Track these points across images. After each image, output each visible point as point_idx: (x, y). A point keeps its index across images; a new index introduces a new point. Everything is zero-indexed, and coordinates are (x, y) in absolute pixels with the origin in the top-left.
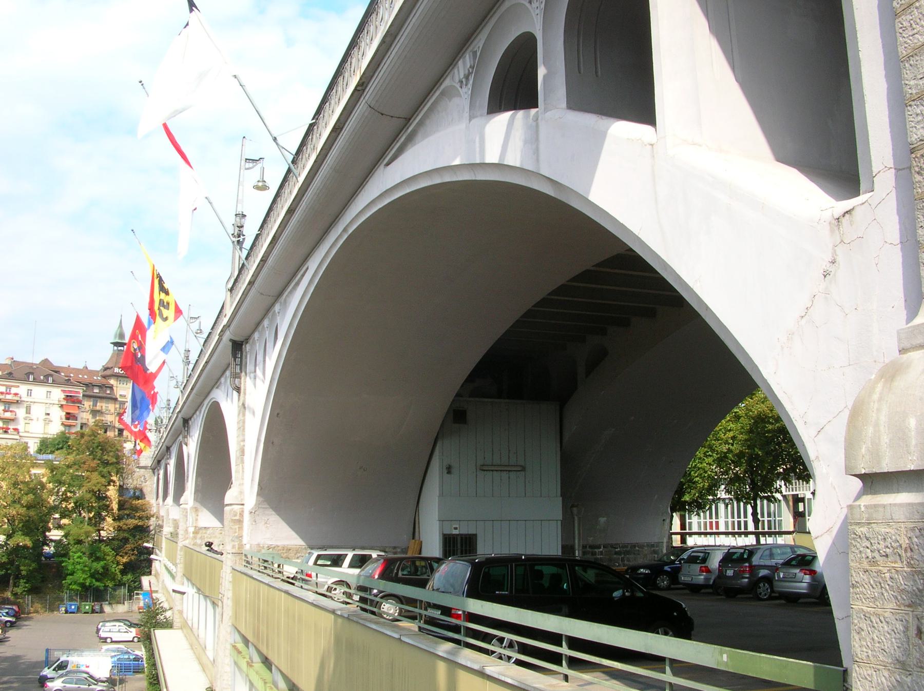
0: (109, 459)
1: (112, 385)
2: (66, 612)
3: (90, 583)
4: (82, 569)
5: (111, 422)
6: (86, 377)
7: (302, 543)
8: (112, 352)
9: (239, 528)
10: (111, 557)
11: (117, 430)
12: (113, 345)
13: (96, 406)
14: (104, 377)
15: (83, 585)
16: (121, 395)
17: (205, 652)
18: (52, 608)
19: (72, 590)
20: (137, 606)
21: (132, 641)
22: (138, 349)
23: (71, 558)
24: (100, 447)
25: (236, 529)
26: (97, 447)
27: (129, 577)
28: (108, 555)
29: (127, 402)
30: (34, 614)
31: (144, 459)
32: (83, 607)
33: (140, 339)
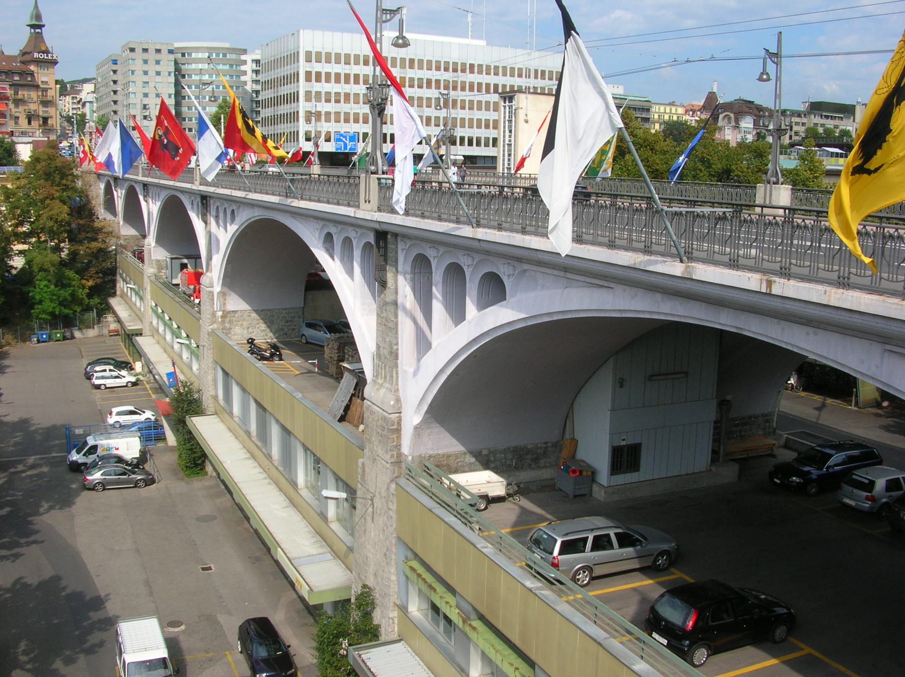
0: (68, 183)
1: (33, 71)
2: (39, 341)
3: (59, 312)
4: (49, 298)
7: (462, 448)
9: (397, 437)
10: (76, 282)
11: (41, 119)
12: (29, 28)
13: (18, 95)
14: (23, 63)
15: (52, 314)
16: (42, 82)
17: (296, 490)
18: (25, 339)
19: (41, 319)
20: (107, 329)
21: (126, 386)
22: (163, 135)
23: (37, 286)
24: (57, 172)
25: (394, 438)
26: (55, 172)
27: (96, 300)
28: (74, 280)
29: (51, 88)
30: (8, 348)
32: (54, 335)
33: (166, 124)
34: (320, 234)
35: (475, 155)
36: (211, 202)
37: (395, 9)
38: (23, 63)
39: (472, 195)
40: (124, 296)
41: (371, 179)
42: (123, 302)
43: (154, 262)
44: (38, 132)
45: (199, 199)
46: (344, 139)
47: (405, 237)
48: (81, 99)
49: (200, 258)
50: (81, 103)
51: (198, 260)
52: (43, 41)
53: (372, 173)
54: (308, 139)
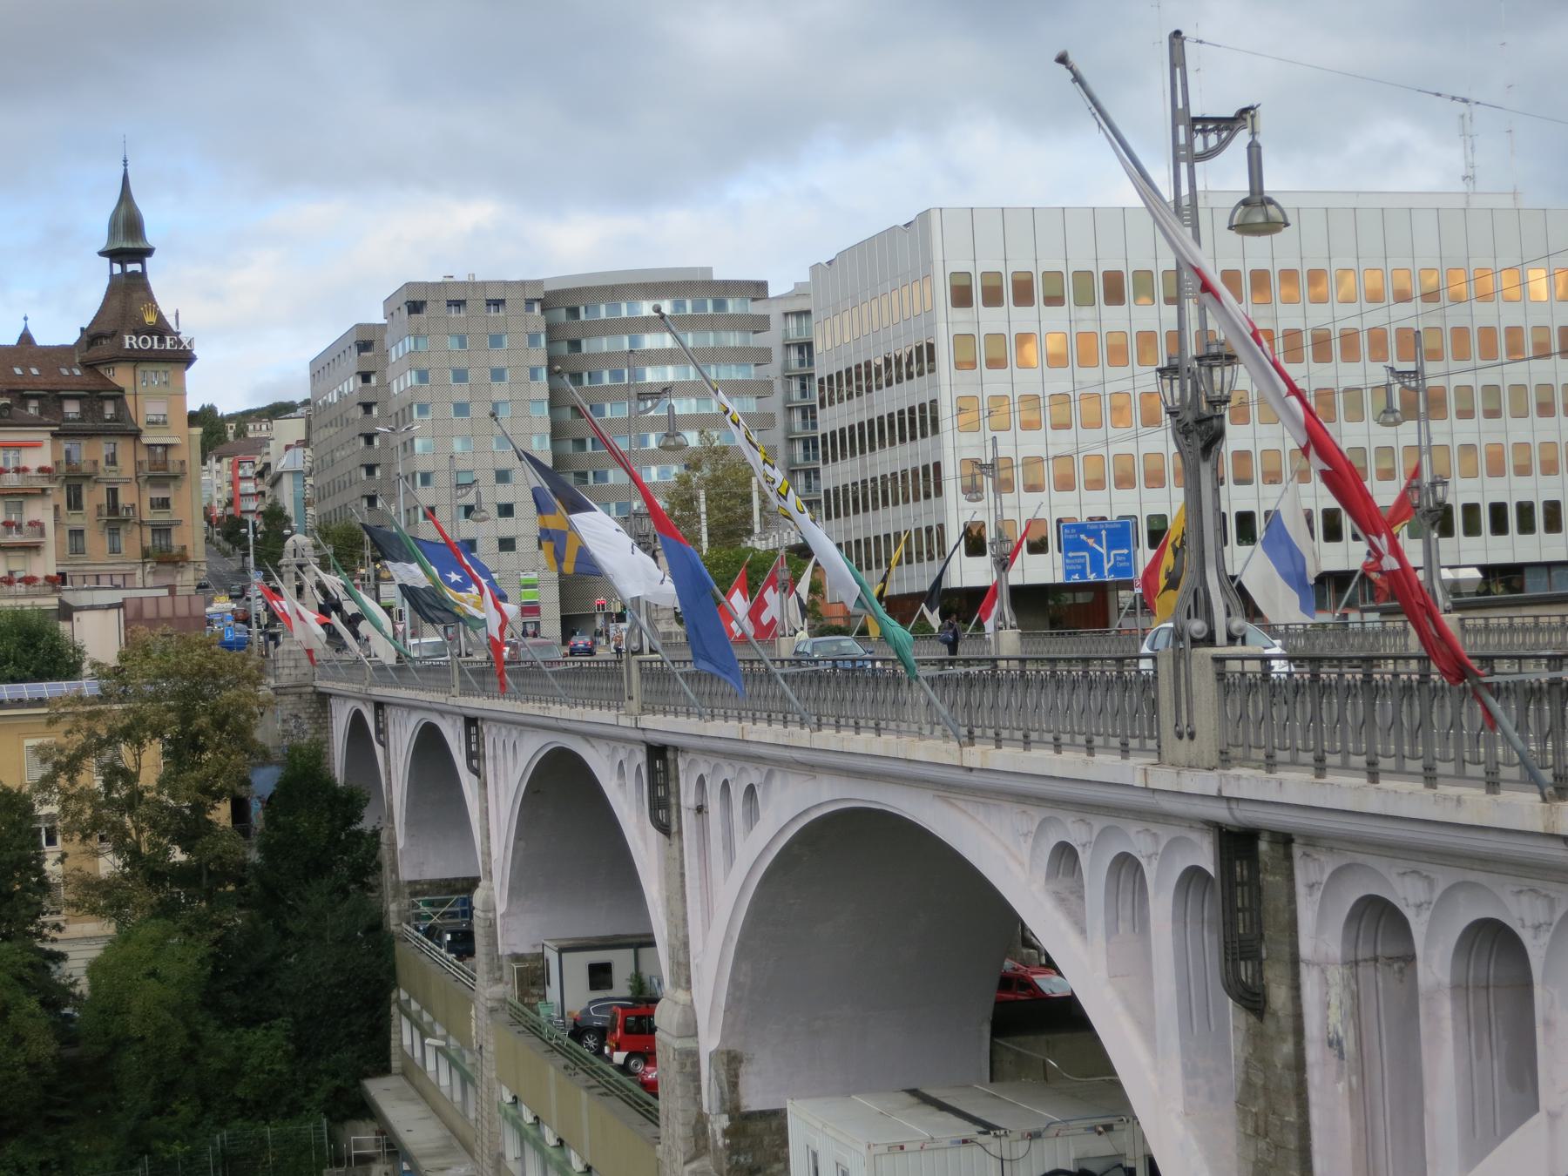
5: (127, 509)
6: (35, 371)
8: (105, 282)
31: (292, 663)
34: (1033, 849)
35: (1519, 559)
36: (681, 764)
37: (1231, 114)
38: (91, 366)
39: (1533, 693)
40: (412, 1072)
41: (1194, 663)
42: (412, 1093)
43: (505, 962)
44: (139, 573)
45: (641, 757)
46: (1091, 542)
47: (1313, 840)
48: (267, 466)
49: (652, 944)
50: (268, 478)
51: (644, 952)
52: (150, 298)
53: (1195, 642)
54: (975, 546)
